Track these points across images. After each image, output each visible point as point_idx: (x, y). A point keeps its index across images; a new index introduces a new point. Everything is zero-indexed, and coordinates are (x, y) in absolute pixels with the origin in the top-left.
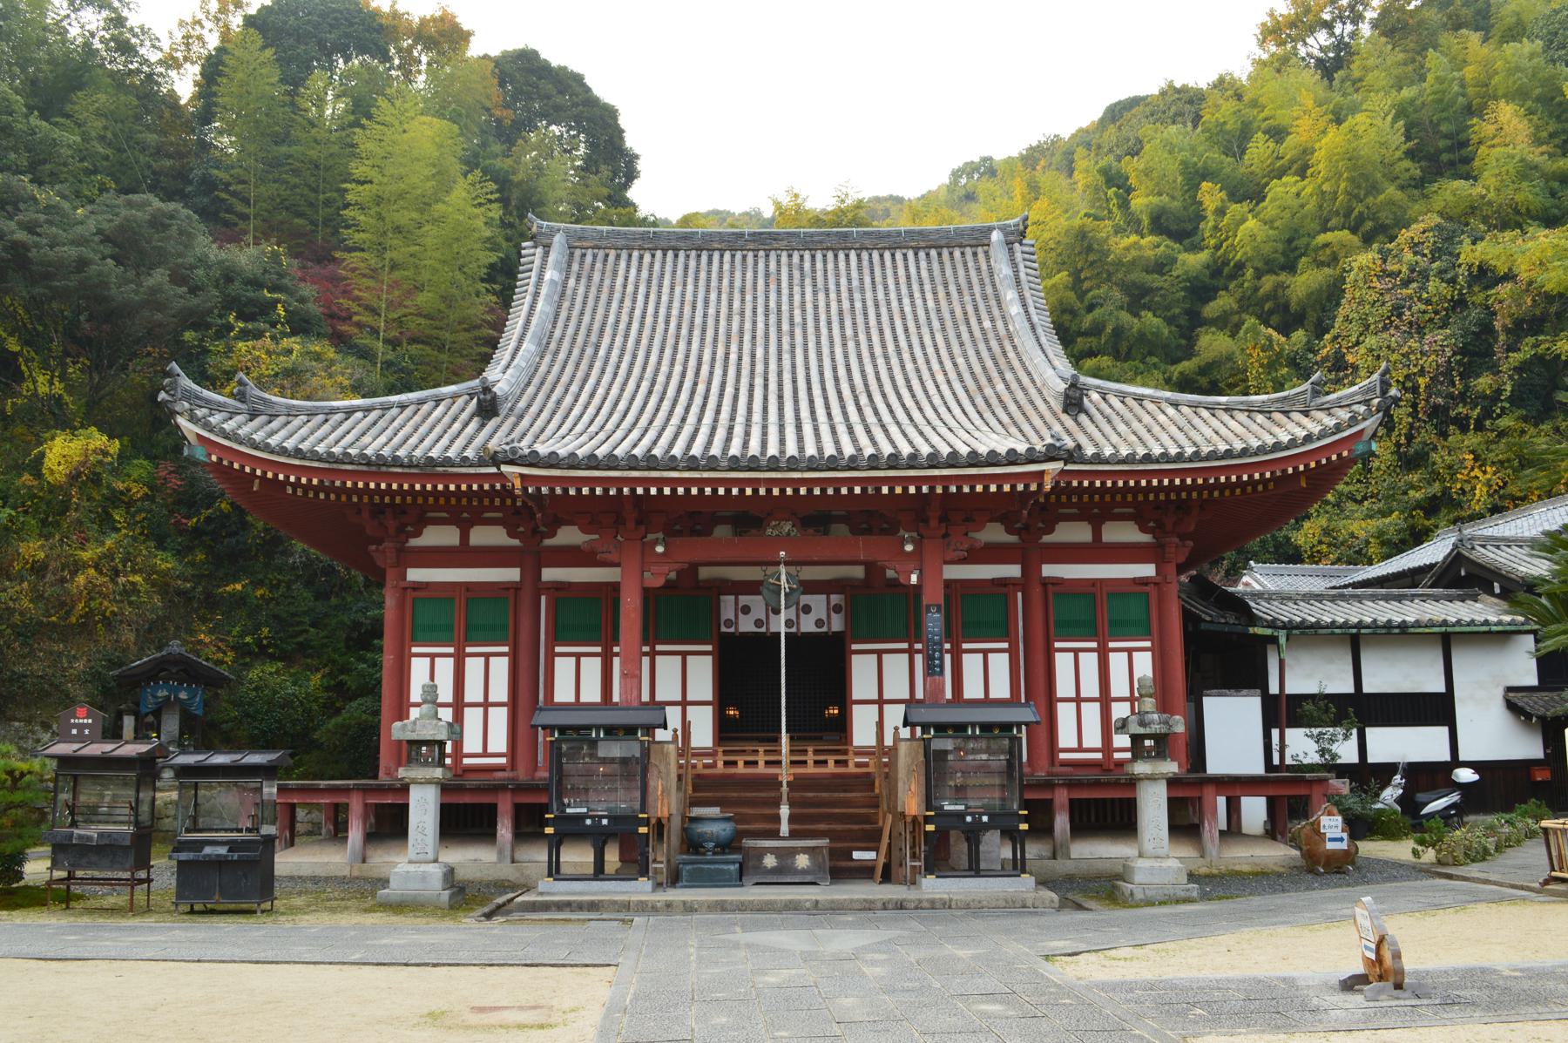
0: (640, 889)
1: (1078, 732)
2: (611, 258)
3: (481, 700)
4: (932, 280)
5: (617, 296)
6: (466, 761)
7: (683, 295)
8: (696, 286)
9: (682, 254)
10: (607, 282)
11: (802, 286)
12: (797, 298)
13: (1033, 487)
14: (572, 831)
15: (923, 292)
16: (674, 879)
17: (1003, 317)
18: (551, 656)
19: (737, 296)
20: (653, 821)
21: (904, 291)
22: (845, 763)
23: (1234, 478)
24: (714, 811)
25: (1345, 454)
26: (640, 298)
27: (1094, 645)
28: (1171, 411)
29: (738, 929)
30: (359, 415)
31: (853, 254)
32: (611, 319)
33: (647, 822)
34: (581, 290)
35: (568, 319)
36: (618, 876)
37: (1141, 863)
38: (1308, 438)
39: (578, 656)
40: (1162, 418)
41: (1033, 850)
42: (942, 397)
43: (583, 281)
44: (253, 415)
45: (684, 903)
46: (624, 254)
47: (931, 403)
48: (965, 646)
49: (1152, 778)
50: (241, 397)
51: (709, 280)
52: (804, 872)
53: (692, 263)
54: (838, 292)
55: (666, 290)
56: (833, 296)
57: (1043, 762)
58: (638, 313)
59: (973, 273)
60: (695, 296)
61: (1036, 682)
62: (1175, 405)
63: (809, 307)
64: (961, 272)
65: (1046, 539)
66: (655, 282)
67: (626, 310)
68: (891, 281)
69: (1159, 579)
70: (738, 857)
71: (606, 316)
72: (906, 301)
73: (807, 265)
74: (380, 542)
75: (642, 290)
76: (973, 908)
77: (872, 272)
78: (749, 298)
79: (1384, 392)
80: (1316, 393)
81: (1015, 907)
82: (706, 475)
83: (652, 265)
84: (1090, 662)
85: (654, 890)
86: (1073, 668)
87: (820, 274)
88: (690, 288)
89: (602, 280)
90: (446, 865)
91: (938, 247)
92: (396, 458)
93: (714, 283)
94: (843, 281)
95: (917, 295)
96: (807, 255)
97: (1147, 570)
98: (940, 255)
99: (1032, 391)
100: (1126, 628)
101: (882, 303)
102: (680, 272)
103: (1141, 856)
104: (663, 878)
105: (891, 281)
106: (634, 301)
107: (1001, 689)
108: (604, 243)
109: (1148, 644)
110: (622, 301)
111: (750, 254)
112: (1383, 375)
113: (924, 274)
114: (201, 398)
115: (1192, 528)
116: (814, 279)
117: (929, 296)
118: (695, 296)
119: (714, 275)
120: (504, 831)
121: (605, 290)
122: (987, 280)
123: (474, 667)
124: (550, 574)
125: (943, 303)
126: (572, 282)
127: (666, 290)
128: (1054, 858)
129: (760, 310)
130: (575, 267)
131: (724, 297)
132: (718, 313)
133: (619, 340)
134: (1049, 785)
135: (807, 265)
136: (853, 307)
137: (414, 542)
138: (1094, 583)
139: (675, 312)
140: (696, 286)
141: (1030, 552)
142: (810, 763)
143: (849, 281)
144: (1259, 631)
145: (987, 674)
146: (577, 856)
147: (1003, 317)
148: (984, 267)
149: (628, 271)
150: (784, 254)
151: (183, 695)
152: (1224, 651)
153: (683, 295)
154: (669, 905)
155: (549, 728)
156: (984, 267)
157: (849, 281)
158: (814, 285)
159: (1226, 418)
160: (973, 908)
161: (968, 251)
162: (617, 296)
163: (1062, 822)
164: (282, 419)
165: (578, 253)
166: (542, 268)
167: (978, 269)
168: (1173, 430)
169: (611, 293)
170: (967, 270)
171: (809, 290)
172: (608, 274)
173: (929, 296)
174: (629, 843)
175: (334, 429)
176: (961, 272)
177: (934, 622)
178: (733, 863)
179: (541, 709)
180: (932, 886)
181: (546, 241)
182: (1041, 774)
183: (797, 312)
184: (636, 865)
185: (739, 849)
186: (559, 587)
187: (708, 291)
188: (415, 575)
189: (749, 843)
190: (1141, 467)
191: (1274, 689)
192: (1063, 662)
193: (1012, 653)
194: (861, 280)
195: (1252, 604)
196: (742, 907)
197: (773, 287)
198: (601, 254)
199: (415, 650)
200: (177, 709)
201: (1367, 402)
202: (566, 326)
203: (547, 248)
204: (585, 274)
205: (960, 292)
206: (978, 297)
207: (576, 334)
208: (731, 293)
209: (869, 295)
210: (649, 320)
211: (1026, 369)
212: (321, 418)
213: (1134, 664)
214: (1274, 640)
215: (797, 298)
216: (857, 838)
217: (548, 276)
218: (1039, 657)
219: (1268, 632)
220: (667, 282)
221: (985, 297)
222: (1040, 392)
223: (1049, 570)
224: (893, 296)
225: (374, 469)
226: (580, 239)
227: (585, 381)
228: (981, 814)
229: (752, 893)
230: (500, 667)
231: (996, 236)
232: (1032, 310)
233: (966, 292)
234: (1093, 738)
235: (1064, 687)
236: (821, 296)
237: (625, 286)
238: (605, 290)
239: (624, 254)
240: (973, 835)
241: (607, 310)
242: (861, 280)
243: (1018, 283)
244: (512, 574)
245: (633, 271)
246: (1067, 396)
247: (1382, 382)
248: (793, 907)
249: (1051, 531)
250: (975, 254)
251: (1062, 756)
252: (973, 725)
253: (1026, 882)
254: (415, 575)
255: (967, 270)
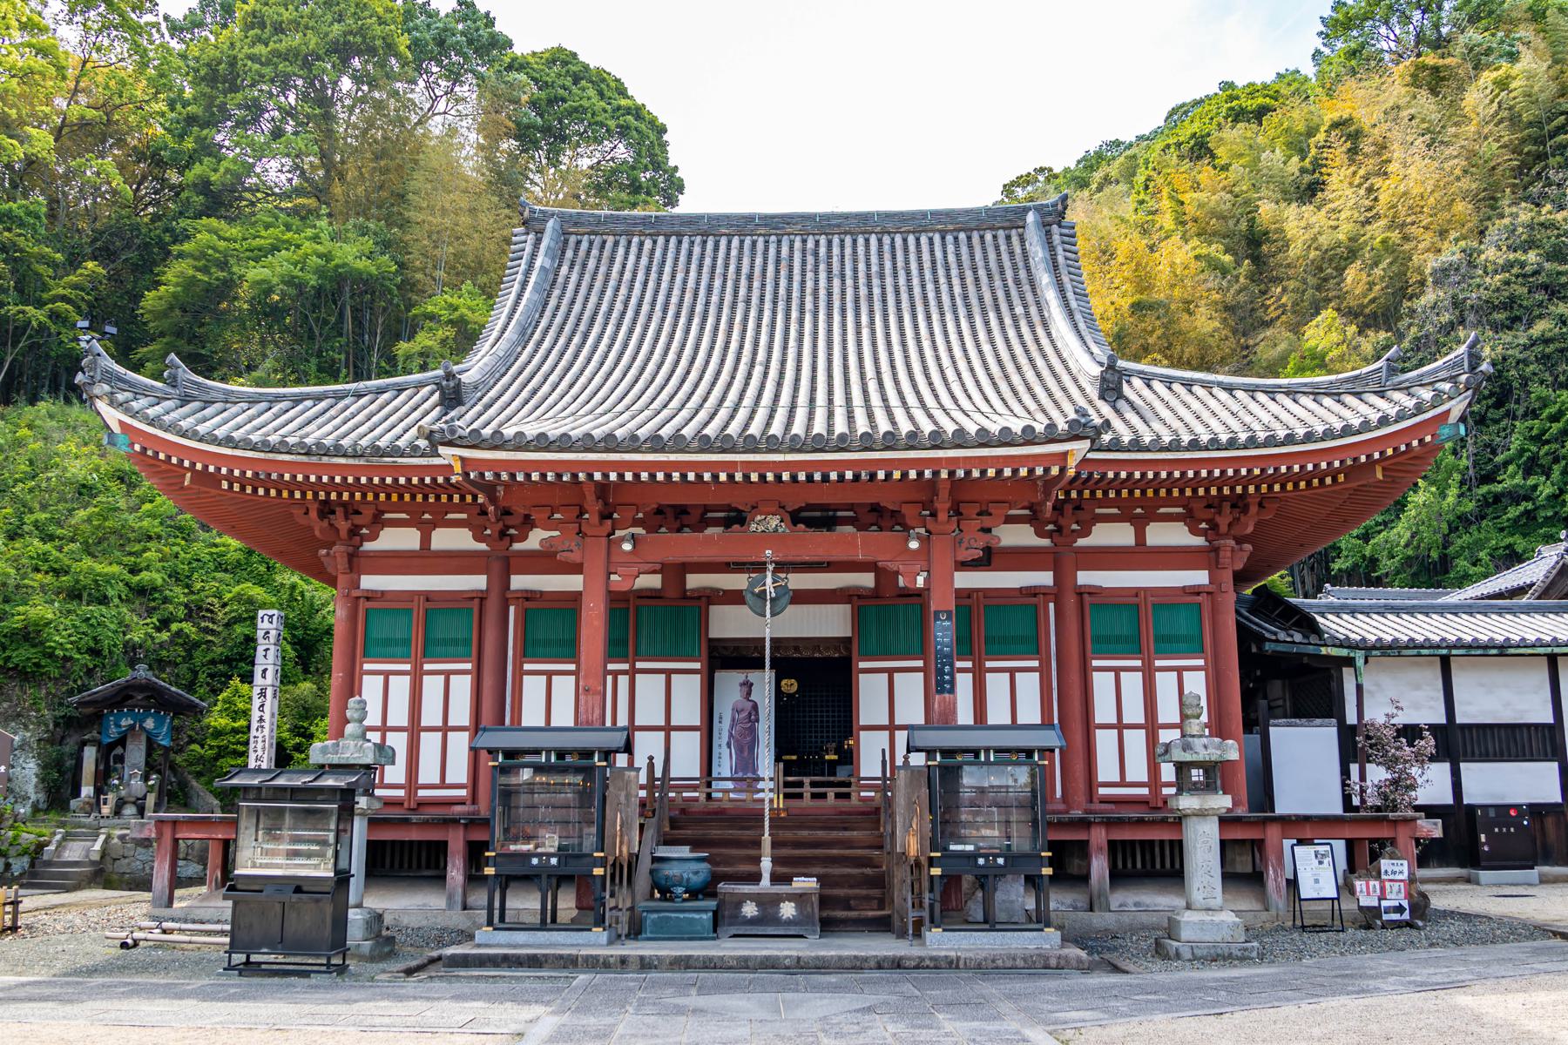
0: (595, 942)
1: (1120, 763)
2: (609, 245)
3: (440, 723)
4: (960, 265)
5: (612, 283)
6: (421, 793)
7: (685, 282)
8: (700, 273)
9: (686, 240)
10: (603, 269)
11: (816, 272)
12: (810, 284)
13: (1055, 471)
14: (519, 875)
15: (948, 277)
16: (636, 931)
17: (1038, 303)
18: (520, 674)
19: (743, 282)
20: (611, 860)
21: (928, 275)
22: (847, 796)
23: (1296, 468)
24: (684, 851)
25: (1428, 439)
26: (638, 286)
27: (1138, 663)
28: (1223, 395)
29: (693, 991)
30: (309, 403)
31: (873, 239)
32: (604, 307)
33: (603, 862)
34: (574, 277)
35: (557, 308)
36: (575, 926)
37: (1188, 917)
38: (1384, 421)
39: (549, 675)
40: (1212, 403)
41: (1060, 901)
42: (963, 385)
43: (577, 268)
44: (185, 400)
45: (642, 958)
46: (623, 241)
47: (949, 390)
48: (989, 664)
49: (1202, 814)
50: (173, 382)
51: (714, 267)
52: (789, 922)
53: (697, 250)
54: (856, 278)
55: (666, 277)
56: (849, 282)
57: (1080, 797)
58: (634, 301)
59: (1005, 257)
60: (698, 283)
61: (1072, 710)
62: (1230, 389)
63: (822, 293)
64: (992, 256)
65: (1081, 542)
66: (654, 268)
67: (620, 298)
68: (914, 266)
69: (1212, 588)
70: (712, 904)
71: (599, 305)
72: (930, 287)
73: (822, 250)
74: (329, 546)
75: (640, 276)
76: (986, 968)
77: (894, 257)
78: (756, 284)
79: (1473, 368)
80: (1392, 371)
81: (1038, 966)
82: (673, 457)
83: (653, 251)
84: (1133, 683)
85: (610, 943)
86: (1114, 690)
87: (835, 260)
88: (693, 274)
89: (597, 268)
90: (371, 911)
91: (968, 230)
92: (337, 447)
93: (719, 270)
94: (862, 266)
95: (942, 280)
96: (823, 240)
97: (1200, 577)
98: (969, 238)
99: (1066, 378)
100: (1171, 644)
101: (903, 289)
102: (683, 258)
103: (1188, 907)
104: (624, 929)
105: (914, 266)
106: (631, 289)
107: (1030, 713)
108: (601, 229)
109: (1201, 662)
110: (617, 289)
111: (761, 239)
112: (1472, 347)
113: (951, 258)
114: (120, 380)
115: (1250, 529)
116: (829, 265)
117: (956, 281)
118: (698, 283)
119: (720, 262)
120: (455, 873)
121: (600, 277)
122: (1021, 265)
123: (432, 687)
124: (519, 582)
125: (971, 289)
126: (564, 270)
127: (666, 277)
128: (1091, 910)
129: (768, 297)
130: (569, 254)
131: (730, 284)
132: (722, 300)
133: (610, 329)
134: (1084, 824)
135: (822, 250)
136: (870, 294)
137: (368, 546)
138: (1136, 592)
139: (674, 300)
140: (700, 273)
141: (1061, 558)
142: (807, 795)
143: (868, 266)
144: (1334, 652)
145: (1015, 697)
146: (524, 903)
147: (1038, 303)
148: (1018, 250)
149: (626, 258)
150: (798, 238)
151: (150, 724)
152: (1286, 677)
153: (685, 282)
154: (623, 961)
155: (492, 752)
156: (1018, 250)
157: (868, 266)
158: (829, 271)
159: (1287, 401)
160: (986, 968)
161: (1001, 233)
162: (612, 283)
163: (1099, 866)
164: (218, 406)
165: (573, 239)
166: (533, 256)
167: (1011, 253)
168: (1225, 415)
169: (606, 281)
170: (999, 254)
171: (823, 276)
172: (604, 261)
173: (956, 281)
174: (582, 883)
175: (277, 417)
176: (992, 256)
177: (943, 632)
178: (706, 911)
179: (485, 730)
180: (939, 942)
181: (538, 227)
182: (1077, 813)
183: (809, 299)
184: (592, 913)
185: (714, 895)
186: (529, 596)
187: (712, 278)
188: (369, 582)
189: (723, 887)
190: (1188, 455)
191: (1351, 718)
192: (1102, 684)
193: (1044, 672)
194: (881, 266)
195: (1319, 619)
196: (710, 965)
197: (783, 273)
198: (598, 240)
199: (367, 667)
200: (144, 738)
201: (1453, 379)
202: (554, 316)
203: (542, 232)
204: (579, 261)
205: (990, 276)
206: (1010, 282)
207: (564, 323)
208: (737, 280)
209: (889, 280)
210: (645, 308)
211: (1060, 356)
212: (264, 405)
213: (1185, 684)
214: (1350, 662)
215: (810, 284)
216: (866, 884)
217: (538, 263)
218: (1074, 677)
219: (1344, 652)
220: (668, 269)
221: (1017, 282)
222: (1075, 380)
223: (1085, 578)
224: (916, 281)
225: (314, 459)
226: (576, 224)
227: (568, 370)
228: (996, 856)
229: (728, 948)
230: (462, 687)
231: (1031, 217)
232: (1070, 295)
233: (997, 277)
234: (1138, 770)
235: (1104, 711)
236: (836, 282)
237: (622, 274)
238: (600, 277)
239: (623, 241)
240: (986, 881)
241: (601, 299)
242: (881, 266)
243: (1056, 267)
244: (478, 582)
245: (632, 258)
246: (1103, 379)
247: (1470, 355)
248: (770, 964)
249: (1087, 533)
250: (1008, 238)
251: (1102, 791)
252: (987, 750)
253: (1048, 941)
254: (369, 582)
255: (999, 254)
